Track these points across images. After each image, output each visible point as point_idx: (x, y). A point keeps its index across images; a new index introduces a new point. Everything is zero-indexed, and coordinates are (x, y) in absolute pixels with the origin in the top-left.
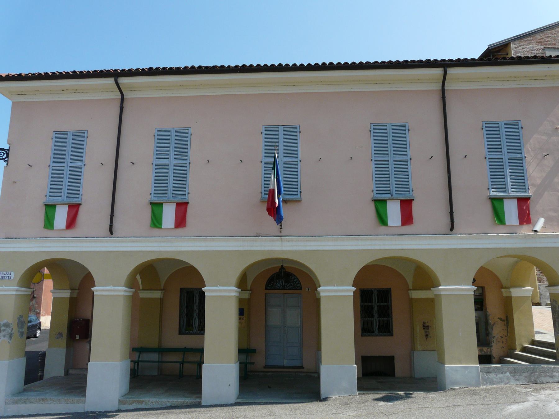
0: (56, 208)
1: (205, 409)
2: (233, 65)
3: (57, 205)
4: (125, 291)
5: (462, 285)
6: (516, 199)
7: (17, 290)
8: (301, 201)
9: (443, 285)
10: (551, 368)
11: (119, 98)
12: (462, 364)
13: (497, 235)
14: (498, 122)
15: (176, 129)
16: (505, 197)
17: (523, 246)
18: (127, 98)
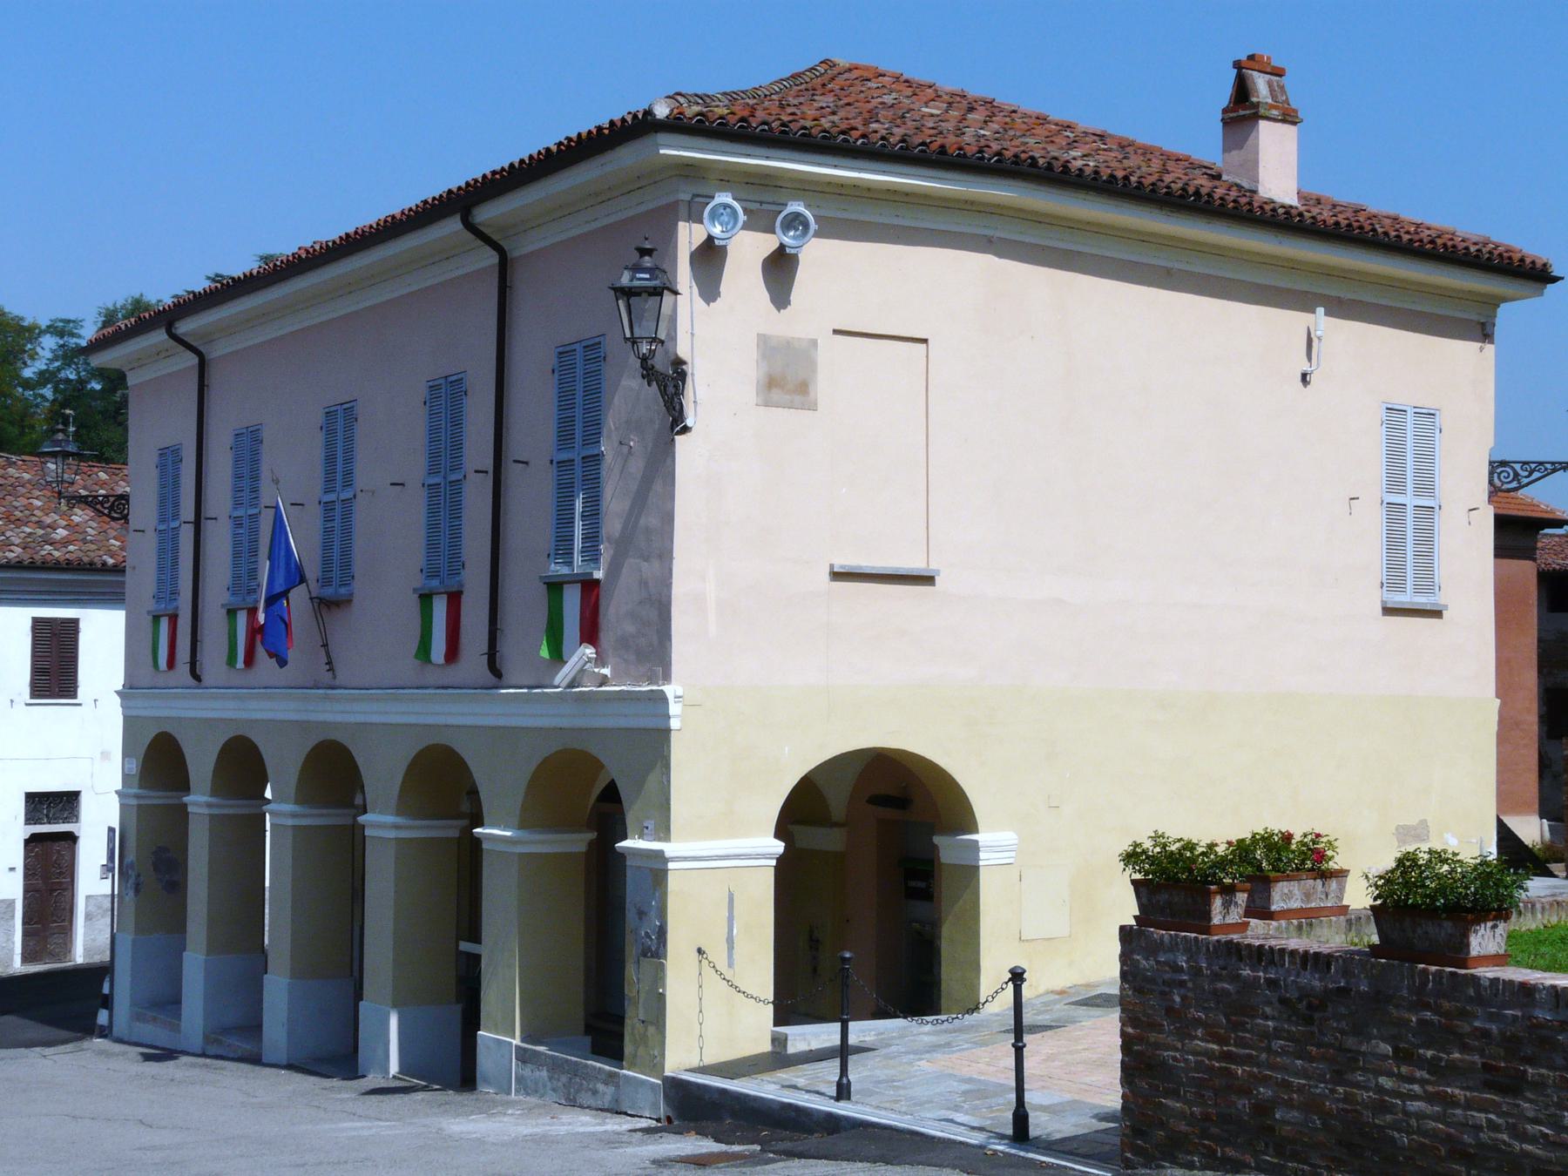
0: (434, 608)
1: (267, 1071)
2: (200, 285)
3: (434, 596)
4: (137, 796)
5: (500, 826)
6: (579, 585)
7: (209, 805)
8: (351, 600)
9: (493, 826)
10: (594, 1068)
11: (189, 364)
12: (497, 1034)
13: (526, 691)
14: (573, 347)
15: (584, 344)
16: (566, 579)
17: (580, 722)
18: (213, 359)
